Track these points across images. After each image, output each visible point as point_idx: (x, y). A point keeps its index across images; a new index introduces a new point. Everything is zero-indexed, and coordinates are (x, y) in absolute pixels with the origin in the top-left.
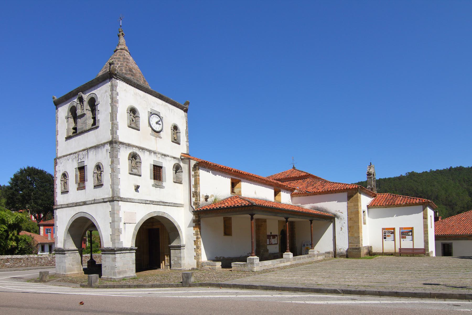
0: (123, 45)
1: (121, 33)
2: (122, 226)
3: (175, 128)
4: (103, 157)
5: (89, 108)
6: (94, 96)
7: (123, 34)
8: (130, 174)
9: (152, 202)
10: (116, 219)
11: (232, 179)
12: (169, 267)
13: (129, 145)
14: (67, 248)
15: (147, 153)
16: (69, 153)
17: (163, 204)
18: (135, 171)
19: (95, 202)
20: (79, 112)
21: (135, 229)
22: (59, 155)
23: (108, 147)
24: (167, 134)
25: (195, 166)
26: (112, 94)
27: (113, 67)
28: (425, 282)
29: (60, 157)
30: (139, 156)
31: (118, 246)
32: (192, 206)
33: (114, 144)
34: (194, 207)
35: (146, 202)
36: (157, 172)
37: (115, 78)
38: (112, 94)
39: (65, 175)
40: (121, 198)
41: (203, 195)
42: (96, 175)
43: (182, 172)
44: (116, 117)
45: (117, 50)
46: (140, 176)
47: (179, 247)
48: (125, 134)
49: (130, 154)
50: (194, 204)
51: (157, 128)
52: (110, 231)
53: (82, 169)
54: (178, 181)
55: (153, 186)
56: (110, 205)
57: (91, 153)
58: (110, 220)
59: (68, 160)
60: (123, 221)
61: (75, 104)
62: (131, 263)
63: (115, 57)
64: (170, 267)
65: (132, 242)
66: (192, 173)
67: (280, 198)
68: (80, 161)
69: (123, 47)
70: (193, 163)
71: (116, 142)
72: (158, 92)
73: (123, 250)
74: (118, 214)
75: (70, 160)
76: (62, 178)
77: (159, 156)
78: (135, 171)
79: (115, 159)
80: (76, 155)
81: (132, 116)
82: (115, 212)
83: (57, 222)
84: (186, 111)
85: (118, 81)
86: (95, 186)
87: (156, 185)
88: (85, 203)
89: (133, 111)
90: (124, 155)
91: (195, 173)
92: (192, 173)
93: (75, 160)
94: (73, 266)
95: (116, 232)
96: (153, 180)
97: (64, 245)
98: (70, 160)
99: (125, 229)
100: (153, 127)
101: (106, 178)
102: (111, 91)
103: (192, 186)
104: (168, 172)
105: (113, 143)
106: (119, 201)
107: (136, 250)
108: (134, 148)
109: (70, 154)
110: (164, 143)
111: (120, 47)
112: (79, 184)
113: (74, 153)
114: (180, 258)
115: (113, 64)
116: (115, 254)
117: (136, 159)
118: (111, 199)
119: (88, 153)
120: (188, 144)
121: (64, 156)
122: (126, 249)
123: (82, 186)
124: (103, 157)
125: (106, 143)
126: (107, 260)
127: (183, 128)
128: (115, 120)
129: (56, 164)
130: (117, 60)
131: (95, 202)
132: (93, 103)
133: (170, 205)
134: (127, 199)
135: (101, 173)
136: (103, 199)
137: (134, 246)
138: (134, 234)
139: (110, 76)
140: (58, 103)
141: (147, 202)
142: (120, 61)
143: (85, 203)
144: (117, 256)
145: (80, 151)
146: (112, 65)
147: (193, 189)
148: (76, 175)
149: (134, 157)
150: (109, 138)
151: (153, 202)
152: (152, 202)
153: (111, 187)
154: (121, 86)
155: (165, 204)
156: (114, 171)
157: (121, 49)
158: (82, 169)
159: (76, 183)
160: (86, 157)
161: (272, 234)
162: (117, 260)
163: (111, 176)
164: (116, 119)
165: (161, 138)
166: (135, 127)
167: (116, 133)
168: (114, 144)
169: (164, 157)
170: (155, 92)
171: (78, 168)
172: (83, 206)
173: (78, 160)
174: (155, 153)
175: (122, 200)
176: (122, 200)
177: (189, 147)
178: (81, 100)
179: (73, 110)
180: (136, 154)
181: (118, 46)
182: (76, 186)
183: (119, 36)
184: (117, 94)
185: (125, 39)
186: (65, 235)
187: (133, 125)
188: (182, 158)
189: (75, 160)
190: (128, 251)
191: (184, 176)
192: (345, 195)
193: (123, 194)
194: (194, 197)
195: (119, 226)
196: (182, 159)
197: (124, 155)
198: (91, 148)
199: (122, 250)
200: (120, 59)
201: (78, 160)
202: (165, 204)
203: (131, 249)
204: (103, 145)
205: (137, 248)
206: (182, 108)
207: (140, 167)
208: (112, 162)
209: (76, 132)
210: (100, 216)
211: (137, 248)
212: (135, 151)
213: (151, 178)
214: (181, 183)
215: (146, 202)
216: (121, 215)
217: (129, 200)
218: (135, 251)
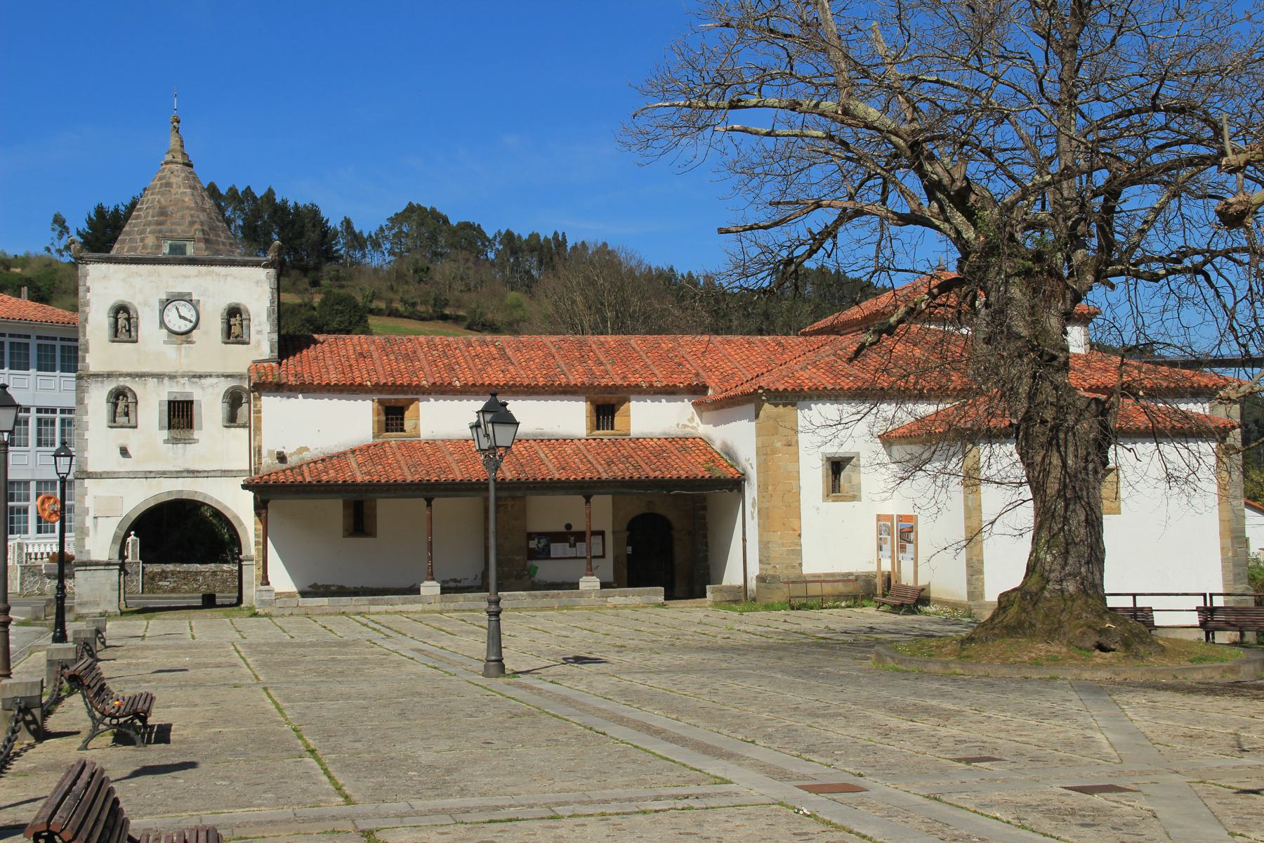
2: (89, 522)
9: (164, 474)
11: (380, 402)
15: (152, 382)
28: (181, 777)
35: (148, 475)
36: (180, 415)
41: (270, 452)
55: (167, 442)
60: (92, 514)
62: (108, 588)
67: (629, 422)
96: (166, 432)
122: (97, 563)
152: (164, 474)
155: (194, 473)
161: (574, 529)
164: (85, 335)
167: (84, 360)
174: (172, 377)
175: (91, 476)
176: (91, 476)
192: (751, 408)
202: (194, 473)
213: (161, 428)
215: (148, 475)
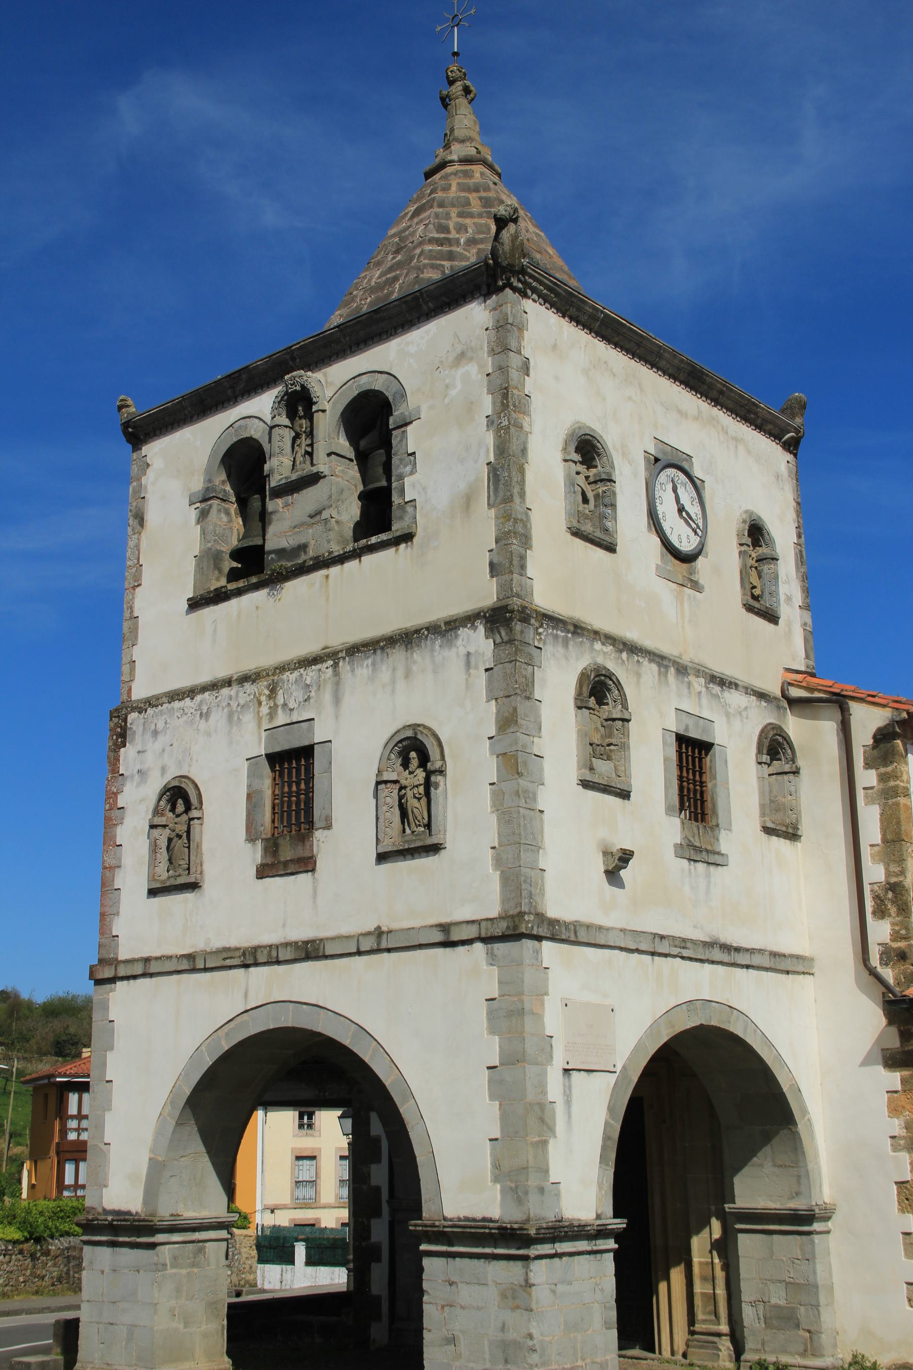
0: (470, 139)
1: (458, 87)
3: (756, 532)
4: (449, 696)
5: (343, 444)
6: (379, 384)
7: (467, 90)
8: (586, 784)
10: (530, 1046)
12: (725, 1345)
13: (577, 629)
14: (164, 1212)
15: (650, 669)
16: (205, 678)
17: (725, 958)
18: (604, 769)
19: (379, 943)
20: (280, 466)
21: (611, 1109)
22: (139, 692)
23: (478, 642)
24: (723, 561)
25: (883, 737)
26: (502, 369)
27: (515, 237)
29: (151, 702)
30: (618, 685)
31: (541, 1212)
32: (873, 973)
33: (518, 626)
34: (889, 974)
37: (515, 289)
38: (502, 369)
39: (179, 797)
40: (553, 922)
42: (391, 796)
43: (796, 772)
44: (522, 483)
45: (443, 165)
46: (625, 795)
47: (801, 1221)
48: (557, 573)
49: (583, 676)
50: (885, 962)
51: (685, 541)
52: (486, 1119)
53: (293, 768)
54: (783, 828)
56: (492, 958)
57: (358, 675)
58: (491, 1050)
59: (205, 716)
61: (257, 431)
63: (439, 195)
64: (739, 1350)
65: (600, 1185)
66: (867, 778)
68: (281, 718)
69: (469, 150)
70: (867, 720)
71: (526, 615)
72: (687, 355)
73: (561, 1239)
74: (539, 1017)
75: (218, 718)
76: (157, 812)
77: (698, 683)
78: (604, 769)
79: (522, 707)
80: (262, 687)
81: (581, 480)
82: (527, 1006)
83: (110, 1056)
84: (791, 446)
85: (529, 305)
86: (382, 858)
87: (690, 845)
88: (310, 951)
89: (586, 449)
90: (557, 677)
91: (883, 778)
92: (867, 778)
93: (248, 718)
94: (186, 1325)
95: (524, 1126)
97: (151, 1193)
98: (218, 718)
99: (568, 1102)
100: (668, 532)
101: (466, 806)
102: (492, 352)
103: (866, 853)
104: (739, 778)
105: (505, 619)
106: (539, 938)
107: (618, 1236)
108: (598, 646)
109: (214, 686)
110: (708, 622)
111: (457, 151)
112: (272, 846)
113: (245, 679)
114: (806, 1291)
115: (515, 221)
116: (153, 1246)
117: (601, 702)
118: (500, 928)
119: (336, 673)
120: (807, 617)
121: (175, 696)
123: (287, 853)
124: (449, 696)
125: (469, 619)
126: (465, 1294)
127: (784, 535)
128: (517, 499)
129: (121, 736)
130: (454, 212)
131: (379, 943)
132: (373, 422)
133: (756, 960)
134: (576, 926)
135: (428, 784)
136: (445, 928)
137: (609, 1210)
138: (606, 1138)
139: (492, 276)
140: (139, 433)
141: (663, 948)
142: (471, 215)
143: (310, 951)
144: (540, 1271)
145: (282, 668)
146: (512, 227)
147: (875, 873)
148: (252, 797)
149: (597, 689)
150: (486, 594)
151: (684, 942)
153: (498, 862)
154: (541, 323)
156: (515, 765)
157: (467, 161)
158: (293, 768)
159: (251, 838)
160: (327, 696)
162: (541, 1295)
163: (498, 797)
164: (522, 495)
165: (696, 586)
166: (598, 534)
168: (518, 626)
169: (716, 689)
170: (674, 354)
171: (267, 756)
172: (298, 966)
173: (272, 715)
174: (682, 670)
177: (816, 638)
178: (299, 404)
179: (244, 466)
180: (610, 676)
181: (447, 147)
182: (255, 855)
183: (445, 101)
184: (526, 369)
185: (475, 113)
186: (158, 1133)
187: (588, 528)
188: (795, 692)
189: (248, 718)
190: (583, 1245)
191: (818, 794)
193: (558, 905)
194: (881, 913)
195: (542, 1088)
196: (793, 703)
197: (557, 677)
198: (354, 650)
199: (562, 1232)
200: (468, 203)
201: (272, 715)
203: (601, 1233)
204: (446, 629)
205: (620, 1224)
206: (772, 429)
207: (625, 747)
208: (507, 722)
209: (252, 567)
210: (421, 1031)
211: (620, 1224)
212: (600, 660)
213: (669, 810)
214: (792, 834)
216: (553, 1020)
217: (583, 936)
218: (611, 1244)
